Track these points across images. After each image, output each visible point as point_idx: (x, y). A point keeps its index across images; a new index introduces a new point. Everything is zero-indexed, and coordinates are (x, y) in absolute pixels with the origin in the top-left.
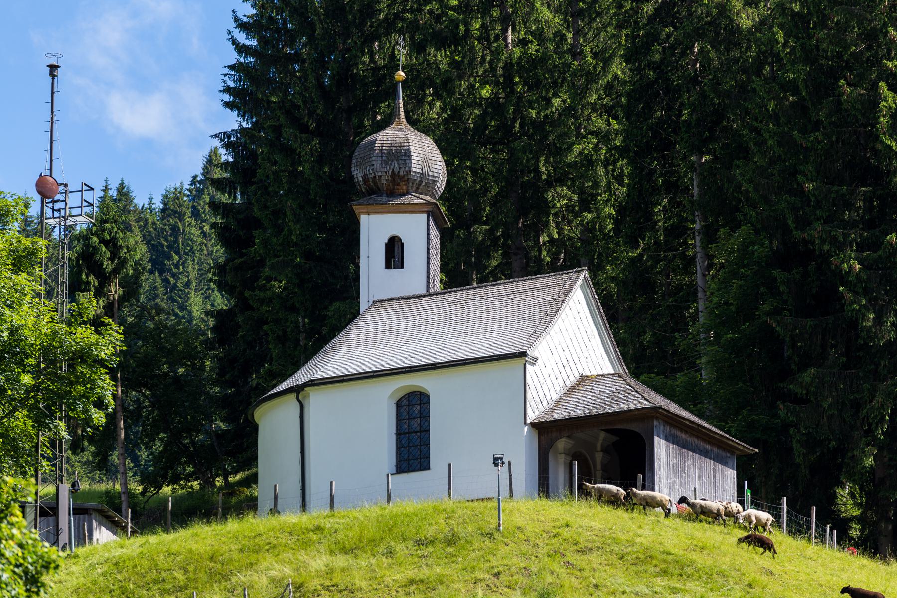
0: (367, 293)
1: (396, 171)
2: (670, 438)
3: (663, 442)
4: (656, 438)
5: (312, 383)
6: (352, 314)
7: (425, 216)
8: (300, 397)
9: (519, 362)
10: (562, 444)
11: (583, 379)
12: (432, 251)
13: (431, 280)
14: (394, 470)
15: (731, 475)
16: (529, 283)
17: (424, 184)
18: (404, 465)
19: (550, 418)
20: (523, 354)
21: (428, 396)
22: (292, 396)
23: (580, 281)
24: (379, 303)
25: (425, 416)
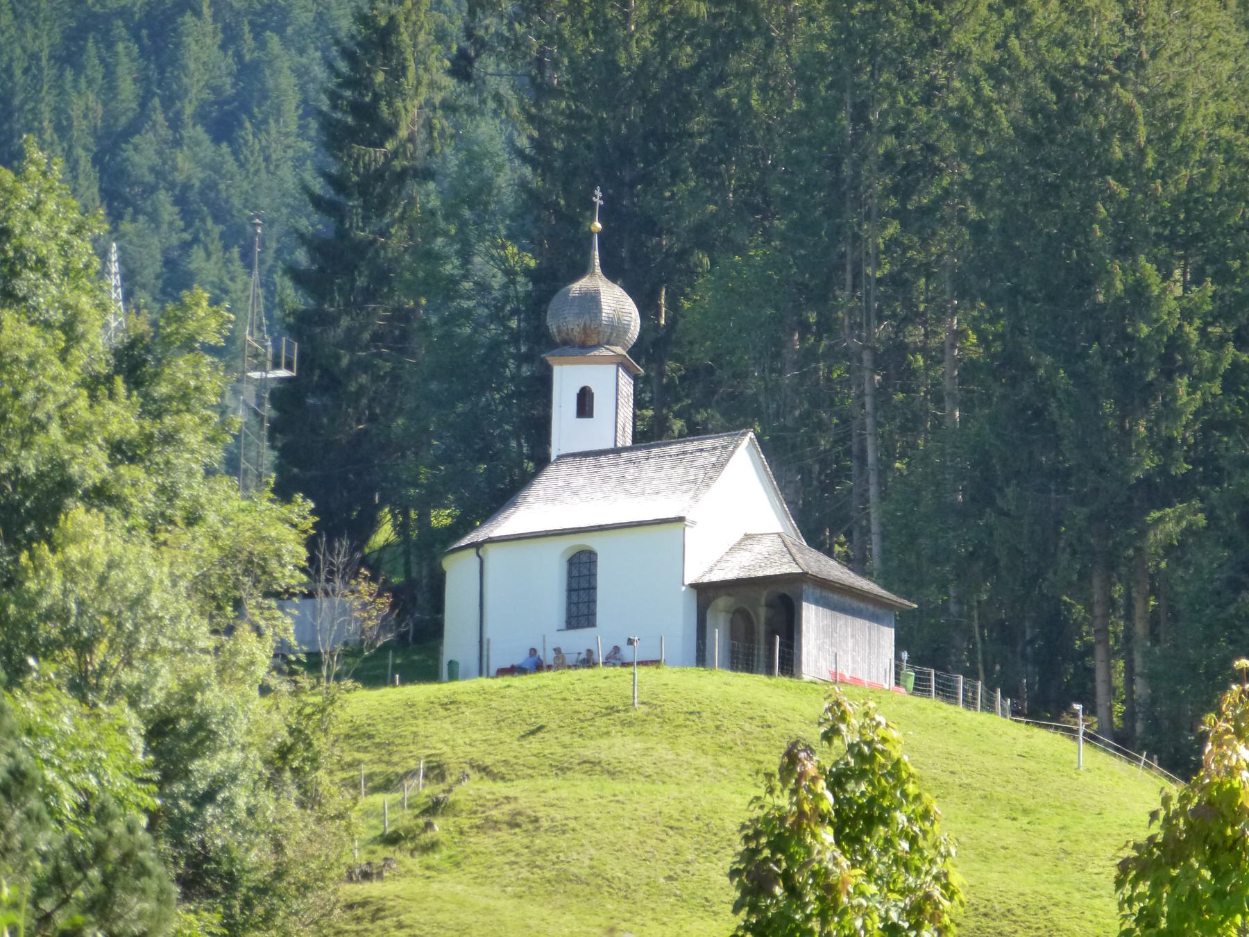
0: (559, 443)
1: (588, 323)
2: (820, 602)
3: (812, 607)
4: (804, 604)
5: (491, 541)
6: (542, 461)
7: (614, 367)
8: (481, 552)
9: (678, 526)
10: (722, 602)
11: (748, 537)
12: (621, 400)
13: (620, 432)
14: (563, 625)
15: (888, 635)
16: (698, 445)
17: (616, 330)
18: (574, 622)
19: (706, 580)
20: (681, 519)
21: (596, 554)
22: (472, 552)
23: (747, 439)
24: (560, 457)
25: (591, 577)
